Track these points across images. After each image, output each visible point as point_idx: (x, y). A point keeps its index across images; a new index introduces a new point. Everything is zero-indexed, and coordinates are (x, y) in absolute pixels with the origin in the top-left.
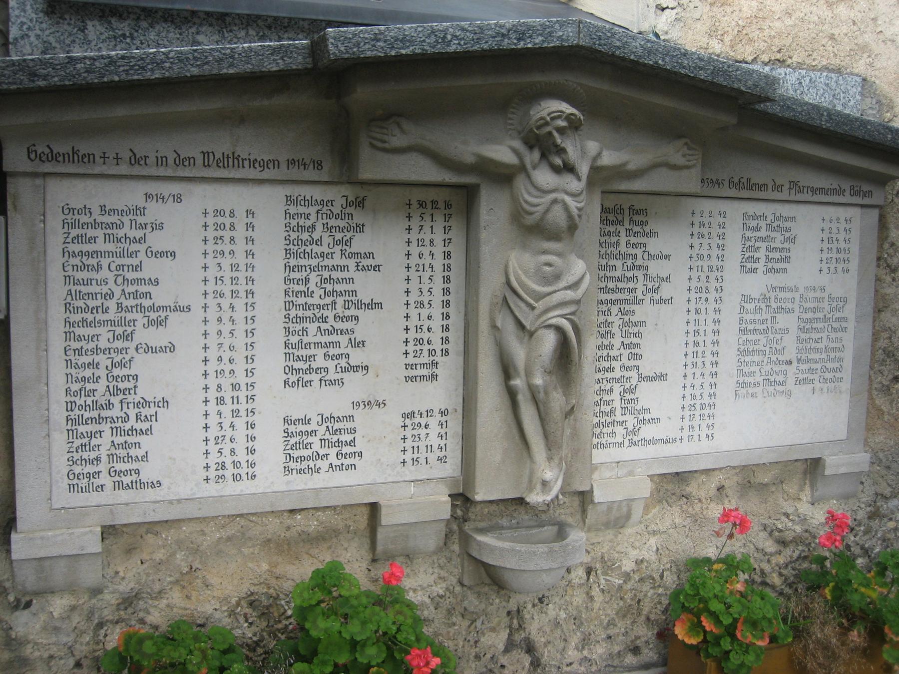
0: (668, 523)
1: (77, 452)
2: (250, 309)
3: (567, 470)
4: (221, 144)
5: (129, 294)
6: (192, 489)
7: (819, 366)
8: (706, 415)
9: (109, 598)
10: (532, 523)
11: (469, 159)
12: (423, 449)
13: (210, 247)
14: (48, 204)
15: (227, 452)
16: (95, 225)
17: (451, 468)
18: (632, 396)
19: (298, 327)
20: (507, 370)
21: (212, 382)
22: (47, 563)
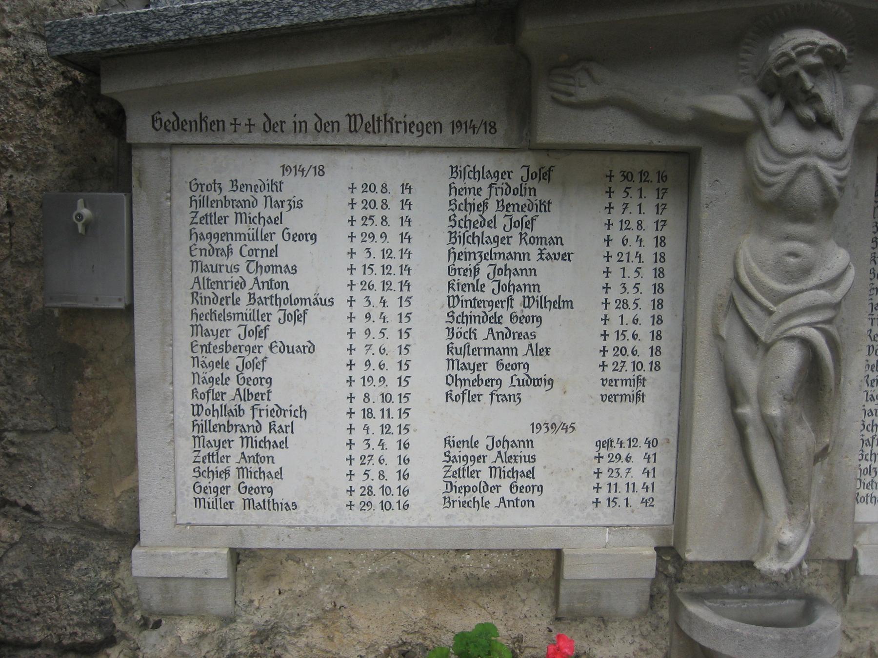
1: (204, 462)
2: (405, 304)
3: (817, 529)
4: (370, 104)
5: (263, 283)
6: (332, 516)
9: (243, 629)
10: (769, 593)
11: (685, 115)
12: (622, 487)
13: (358, 229)
14: (175, 179)
15: (374, 474)
16: (225, 203)
17: (659, 514)
19: (465, 328)
20: (733, 393)
21: (358, 390)
22: (172, 584)
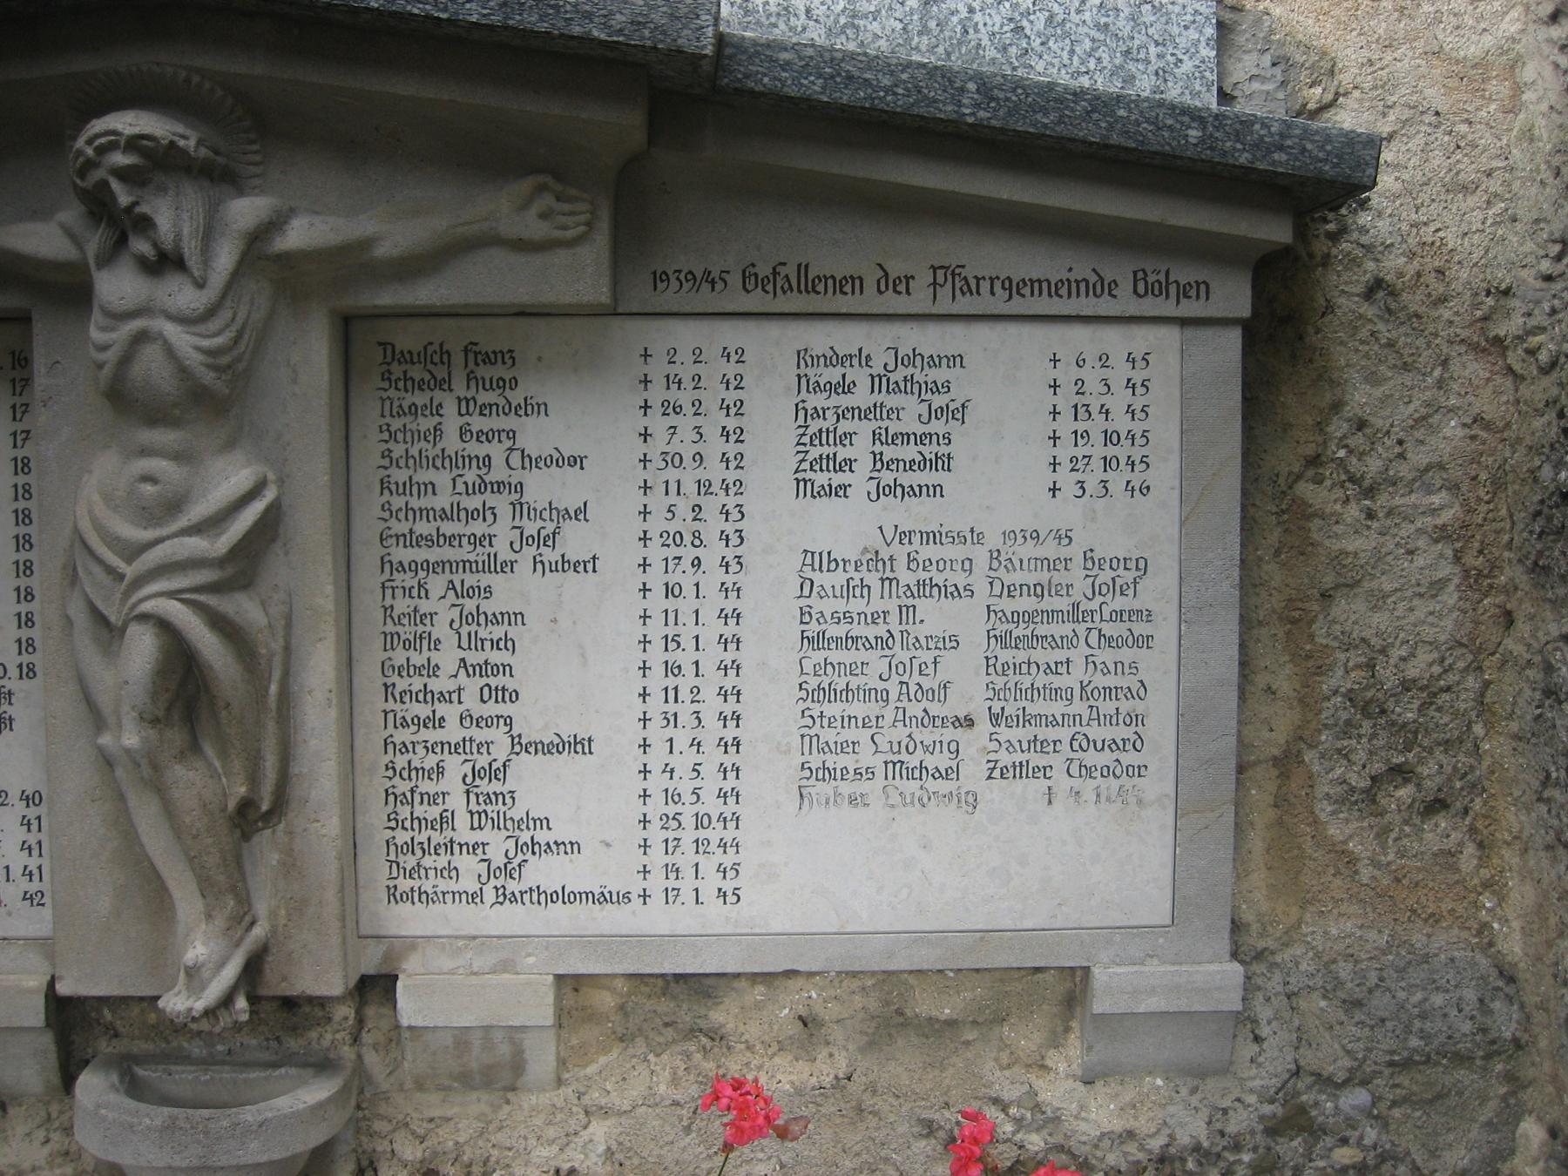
0: (636, 1091)
7: (1064, 734)
8: (715, 842)
10: (266, 1056)
18: (496, 786)
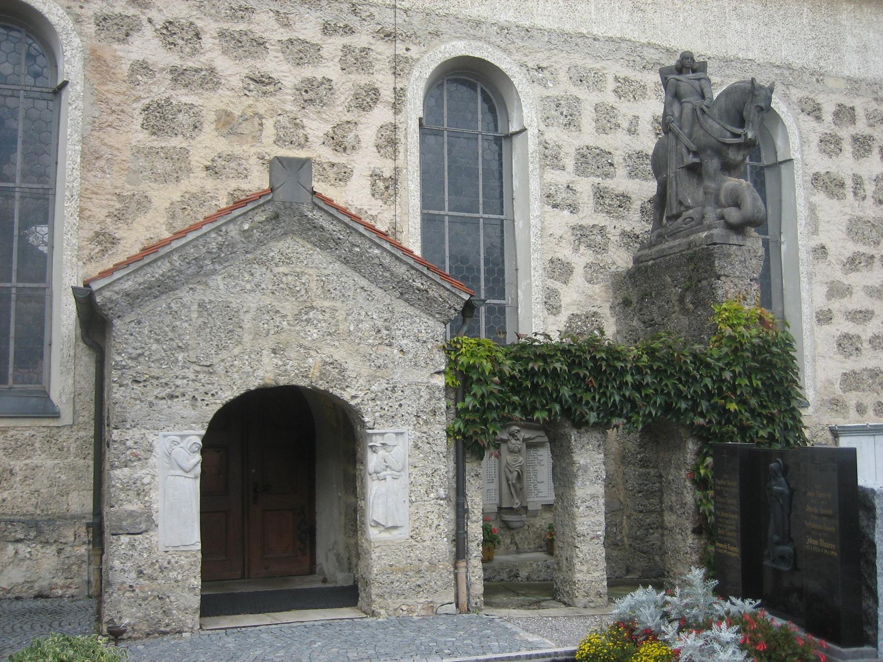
17: (497, 501)
20: (508, 480)
